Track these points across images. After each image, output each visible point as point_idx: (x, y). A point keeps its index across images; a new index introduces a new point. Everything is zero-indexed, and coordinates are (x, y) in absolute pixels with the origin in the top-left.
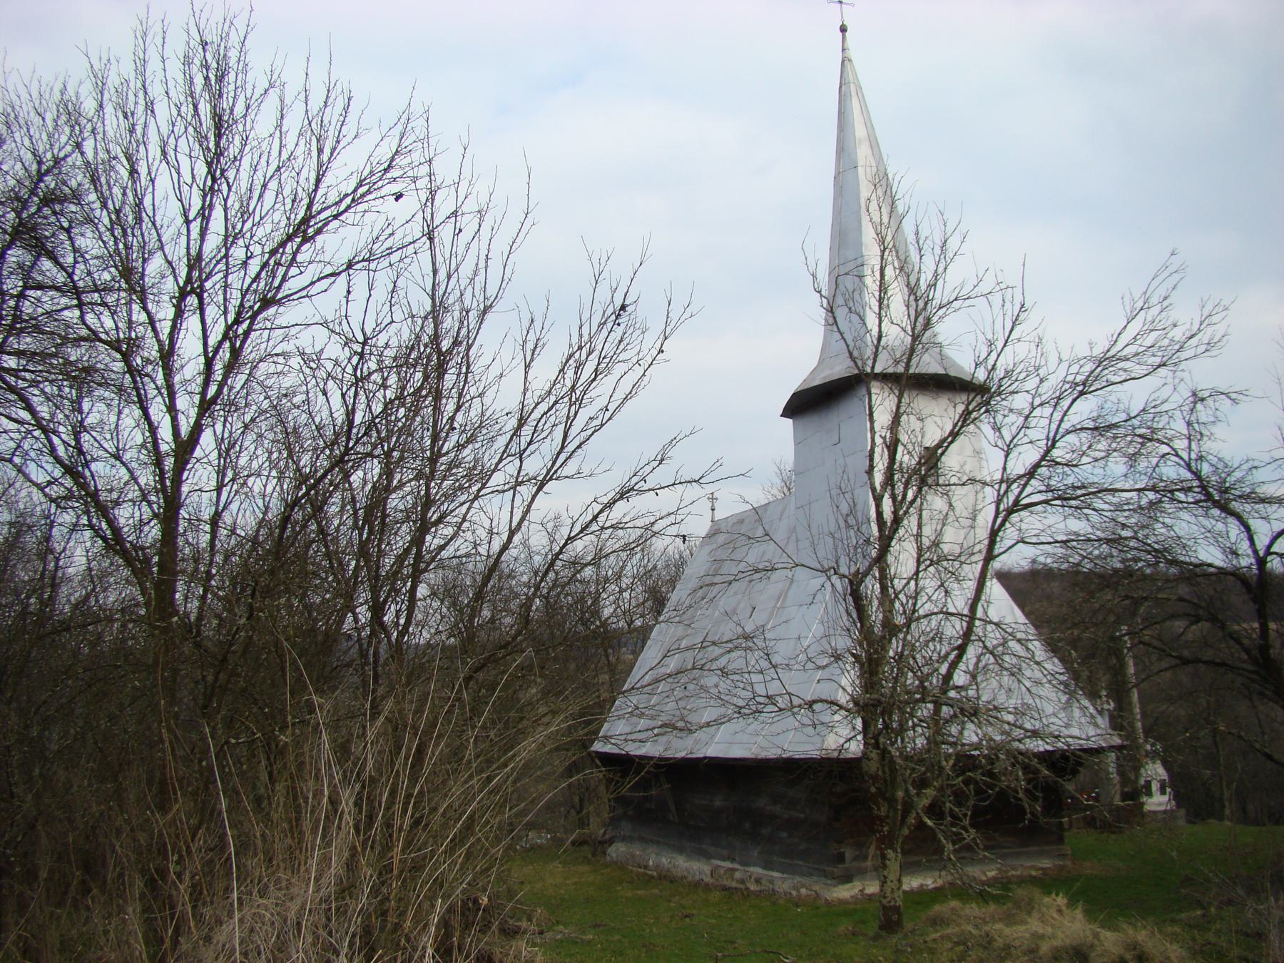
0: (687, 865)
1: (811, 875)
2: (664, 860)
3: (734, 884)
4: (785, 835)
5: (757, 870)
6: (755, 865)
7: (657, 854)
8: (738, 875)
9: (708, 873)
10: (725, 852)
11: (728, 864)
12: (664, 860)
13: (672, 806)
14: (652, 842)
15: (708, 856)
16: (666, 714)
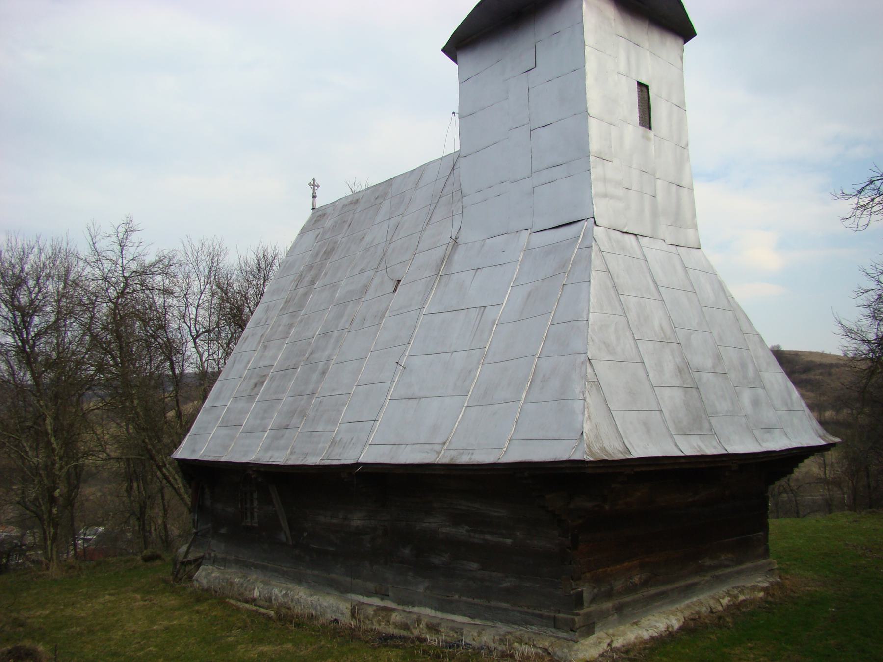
0: (314, 599)
1: (527, 623)
2: (276, 591)
3: (391, 630)
4: (475, 566)
5: (428, 612)
6: (421, 604)
7: (266, 583)
8: (396, 617)
9: (348, 612)
10: (371, 585)
11: (376, 601)
12: (276, 591)
13: (284, 524)
14: (256, 567)
15: (343, 589)
16: (233, 429)
